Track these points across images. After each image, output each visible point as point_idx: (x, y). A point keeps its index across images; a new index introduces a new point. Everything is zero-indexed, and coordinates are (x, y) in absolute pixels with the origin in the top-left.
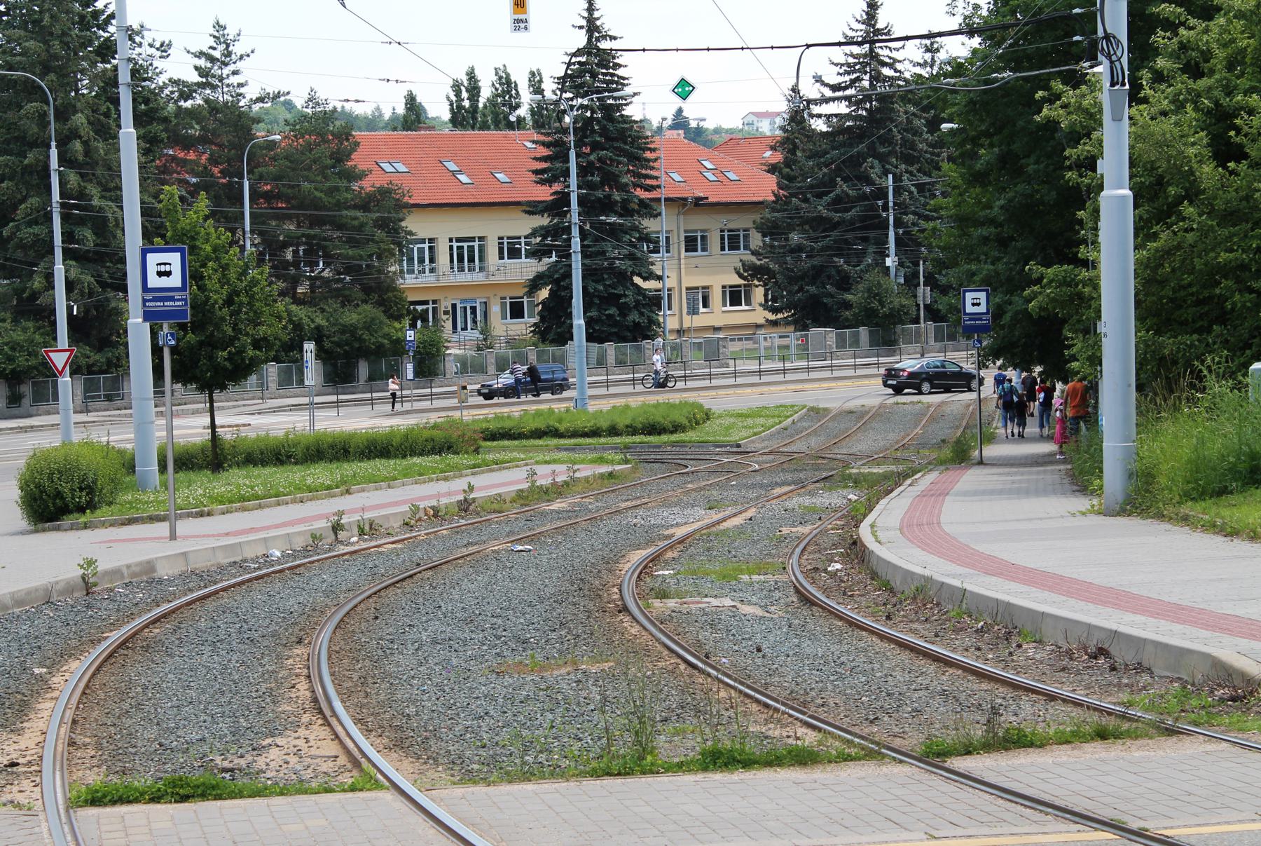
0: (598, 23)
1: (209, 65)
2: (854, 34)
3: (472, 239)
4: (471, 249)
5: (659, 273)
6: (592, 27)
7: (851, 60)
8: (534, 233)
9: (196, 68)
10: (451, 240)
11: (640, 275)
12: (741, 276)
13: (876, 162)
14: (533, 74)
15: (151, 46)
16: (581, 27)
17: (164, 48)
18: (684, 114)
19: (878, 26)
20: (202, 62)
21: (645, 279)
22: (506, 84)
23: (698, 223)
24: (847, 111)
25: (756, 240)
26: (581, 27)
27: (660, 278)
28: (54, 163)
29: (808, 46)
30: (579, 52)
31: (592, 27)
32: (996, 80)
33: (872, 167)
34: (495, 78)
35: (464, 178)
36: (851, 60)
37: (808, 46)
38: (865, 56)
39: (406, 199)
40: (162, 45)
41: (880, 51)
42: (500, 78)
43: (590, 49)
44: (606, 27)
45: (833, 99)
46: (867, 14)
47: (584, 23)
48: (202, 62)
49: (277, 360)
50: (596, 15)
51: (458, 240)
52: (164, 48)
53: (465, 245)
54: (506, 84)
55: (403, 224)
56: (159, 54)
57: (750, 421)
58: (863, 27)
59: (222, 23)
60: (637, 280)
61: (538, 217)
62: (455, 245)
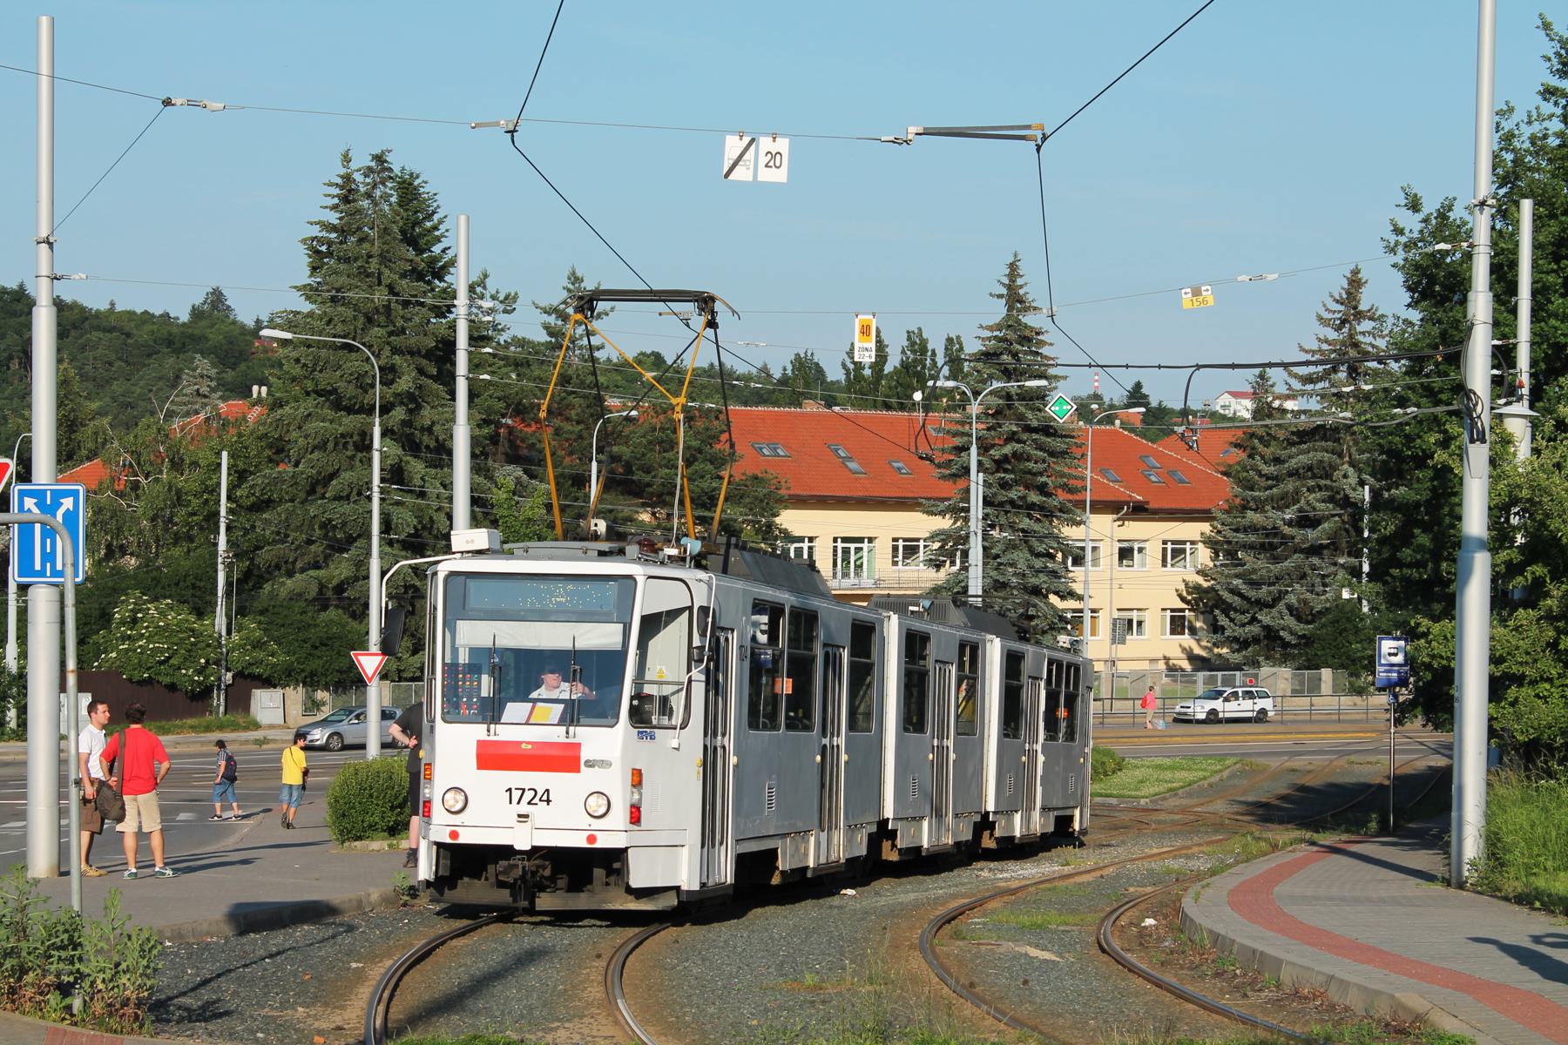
0: (1021, 292)
1: (560, 323)
2: (1331, 316)
3: (861, 540)
4: (846, 551)
5: (1080, 592)
6: (1015, 299)
7: (1325, 347)
8: (933, 537)
9: (547, 327)
10: (835, 540)
11: (1056, 593)
12: (1183, 599)
13: (1351, 471)
14: (950, 340)
15: (493, 298)
16: (1000, 296)
17: (509, 303)
18: (1144, 391)
19: (1361, 308)
20: (552, 320)
21: (1063, 598)
22: (917, 345)
23: (1136, 530)
24: (1318, 407)
25: (1204, 555)
26: (1000, 296)
27: (1080, 598)
28: (377, 431)
29: (1199, 367)
30: (999, 327)
31: (1015, 299)
32: (1393, 417)
33: (1345, 476)
34: (906, 343)
35: (852, 465)
36: (1325, 347)
37: (1199, 367)
38: (1343, 343)
39: (783, 492)
40: (506, 298)
41: (1361, 338)
42: (913, 344)
43: (1011, 323)
44: (1030, 297)
45: (1303, 393)
46: (1349, 293)
47: (1005, 291)
48: (552, 320)
49: (37, 882)
50: (1019, 282)
51: (845, 540)
52: (509, 303)
53: (852, 546)
54: (917, 345)
55: (778, 520)
56: (502, 307)
57: (1168, 775)
58: (1342, 308)
59: (579, 274)
60: (1053, 599)
61: (939, 518)
62: (840, 545)
